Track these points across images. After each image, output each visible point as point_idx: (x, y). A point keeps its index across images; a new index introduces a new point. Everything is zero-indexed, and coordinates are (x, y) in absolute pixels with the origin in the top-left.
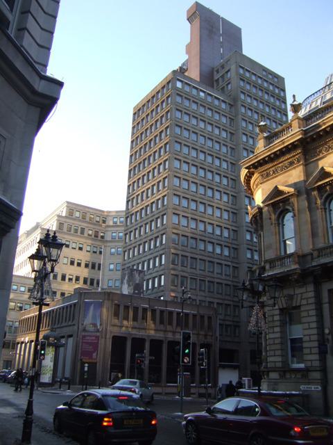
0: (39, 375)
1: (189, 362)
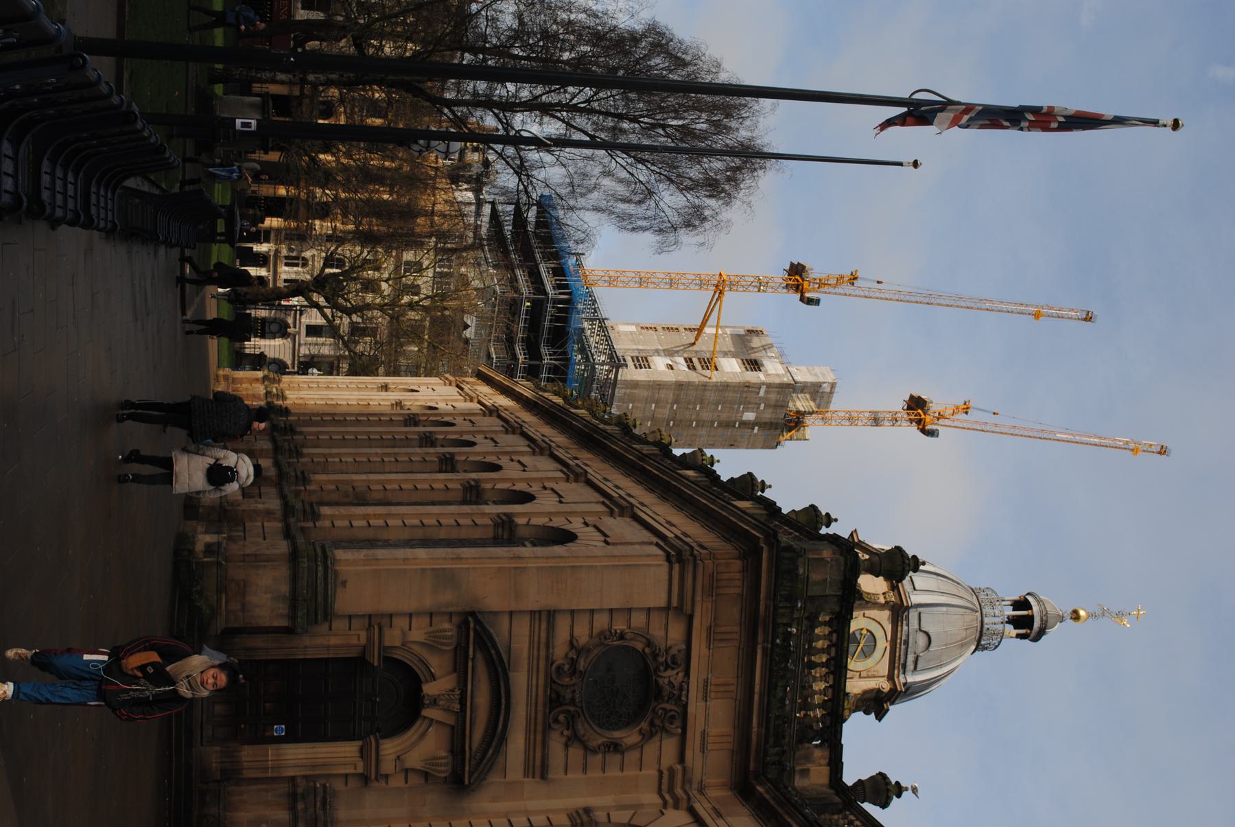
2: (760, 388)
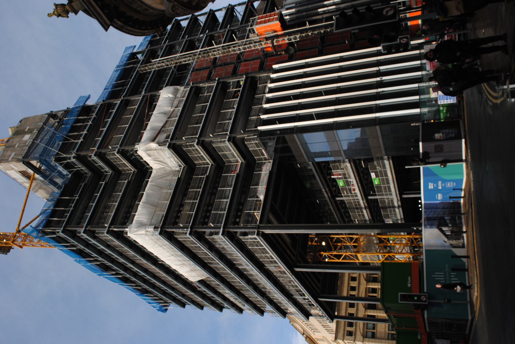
0: (20, 134)
1: (425, 296)
2: (13, 158)
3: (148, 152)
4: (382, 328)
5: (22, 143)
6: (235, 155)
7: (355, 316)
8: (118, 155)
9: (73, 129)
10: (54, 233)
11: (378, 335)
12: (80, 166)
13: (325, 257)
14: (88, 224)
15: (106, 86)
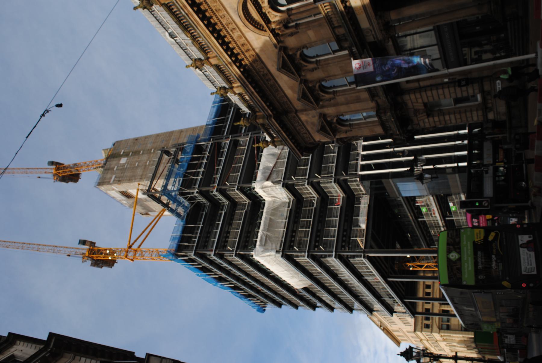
0: (116, 157)
1: (487, 201)
2: (114, 180)
3: (264, 189)
4: (457, 321)
5: (120, 166)
6: (339, 191)
7: (431, 311)
8: (237, 192)
9: (190, 166)
10: (186, 256)
11: (452, 327)
12: (201, 199)
13: (410, 267)
14: (216, 248)
15: (207, 121)
